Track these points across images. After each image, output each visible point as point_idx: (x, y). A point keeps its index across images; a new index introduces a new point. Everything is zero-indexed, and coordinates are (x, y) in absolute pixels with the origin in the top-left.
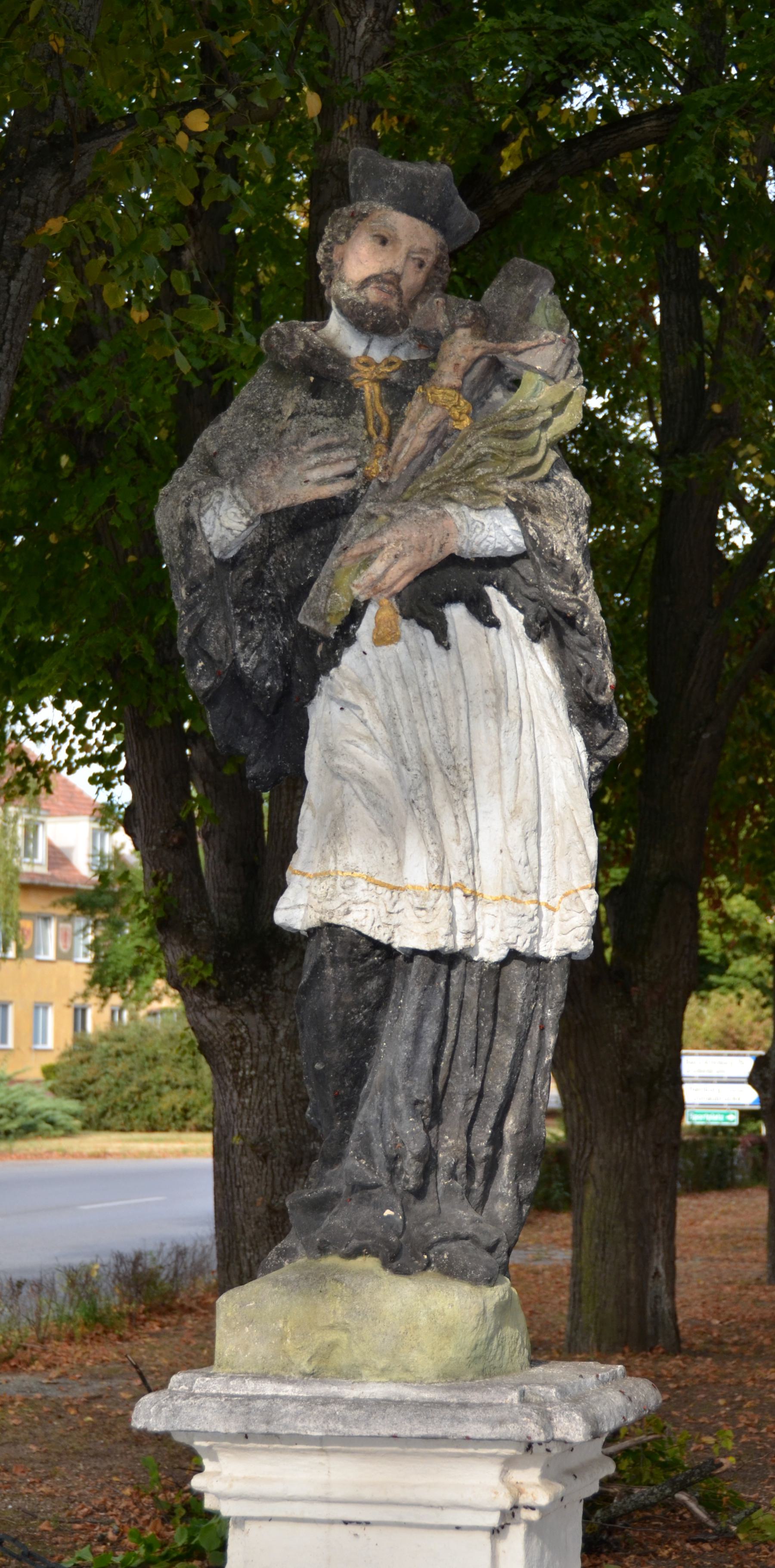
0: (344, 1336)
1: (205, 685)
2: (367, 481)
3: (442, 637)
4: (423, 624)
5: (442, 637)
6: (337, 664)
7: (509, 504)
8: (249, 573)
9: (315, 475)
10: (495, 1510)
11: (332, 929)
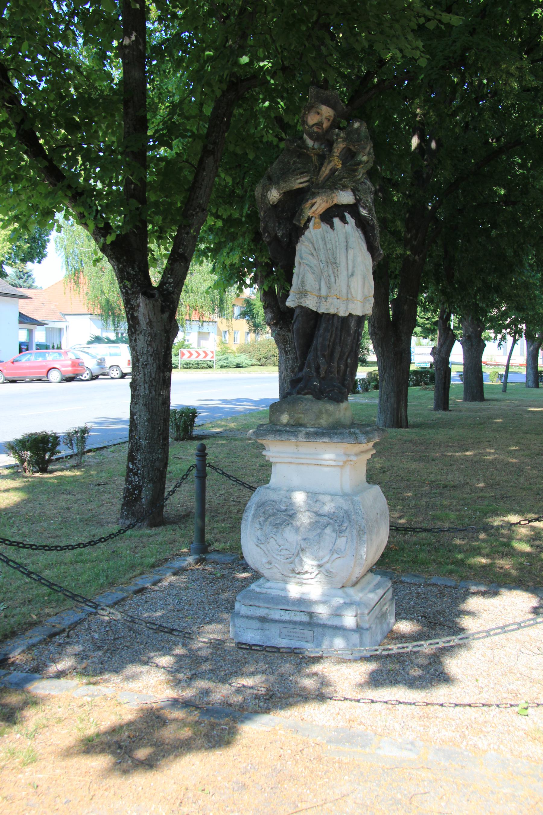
0: (303, 416)
1: (268, 240)
2: (313, 183)
3: (332, 226)
4: (328, 223)
5: (332, 226)
6: (304, 234)
7: (351, 189)
8: (280, 209)
9: (299, 181)
10: (487, 400)
11: (301, 307)
